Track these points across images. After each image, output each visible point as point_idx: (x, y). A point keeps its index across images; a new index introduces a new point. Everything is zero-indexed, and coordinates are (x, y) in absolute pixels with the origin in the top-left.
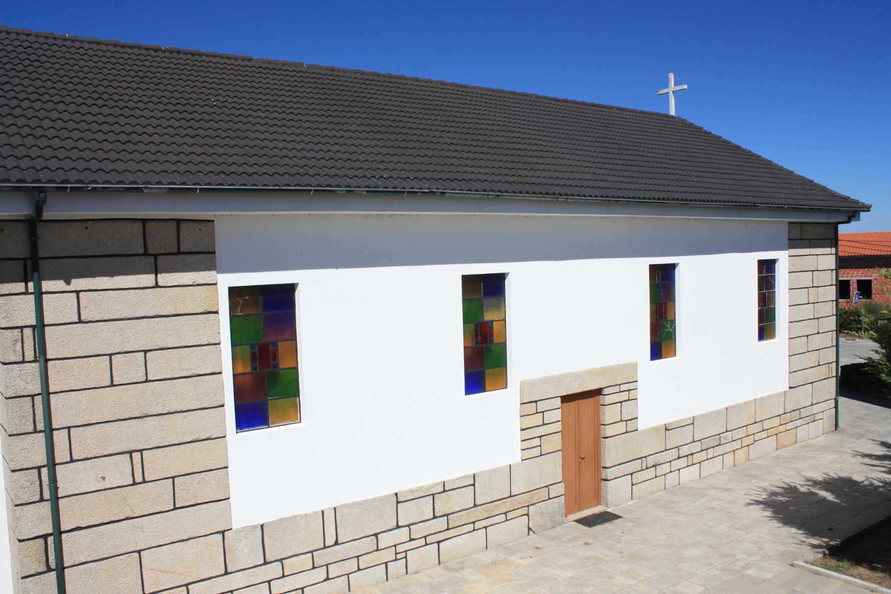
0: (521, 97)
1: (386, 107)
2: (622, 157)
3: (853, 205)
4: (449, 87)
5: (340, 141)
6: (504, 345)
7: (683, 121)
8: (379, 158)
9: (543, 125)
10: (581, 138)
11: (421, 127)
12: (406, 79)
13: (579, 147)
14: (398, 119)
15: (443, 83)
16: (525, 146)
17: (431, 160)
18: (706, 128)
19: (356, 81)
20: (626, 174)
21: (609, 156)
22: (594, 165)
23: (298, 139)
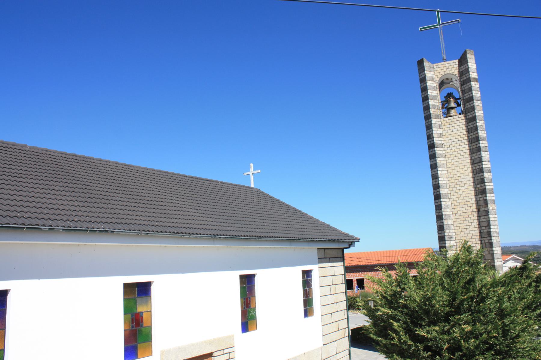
0: (164, 174)
1: (80, 176)
2: (223, 211)
3: (350, 238)
4: (120, 166)
5: (48, 196)
6: (150, 327)
7: (259, 191)
8: (73, 208)
9: (177, 191)
10: (199, 199)
11: (101, 189)
12: (94, 159)
13: (198, 205)
14: (87, 184)
15: (117, 163)
16: (165, 204)
17: (106, 211)
18: (271, 194)
19: (61, 158)
20: (225, 221)
21: (216, 210)
22: (206, 216)
23: (18, 193)
